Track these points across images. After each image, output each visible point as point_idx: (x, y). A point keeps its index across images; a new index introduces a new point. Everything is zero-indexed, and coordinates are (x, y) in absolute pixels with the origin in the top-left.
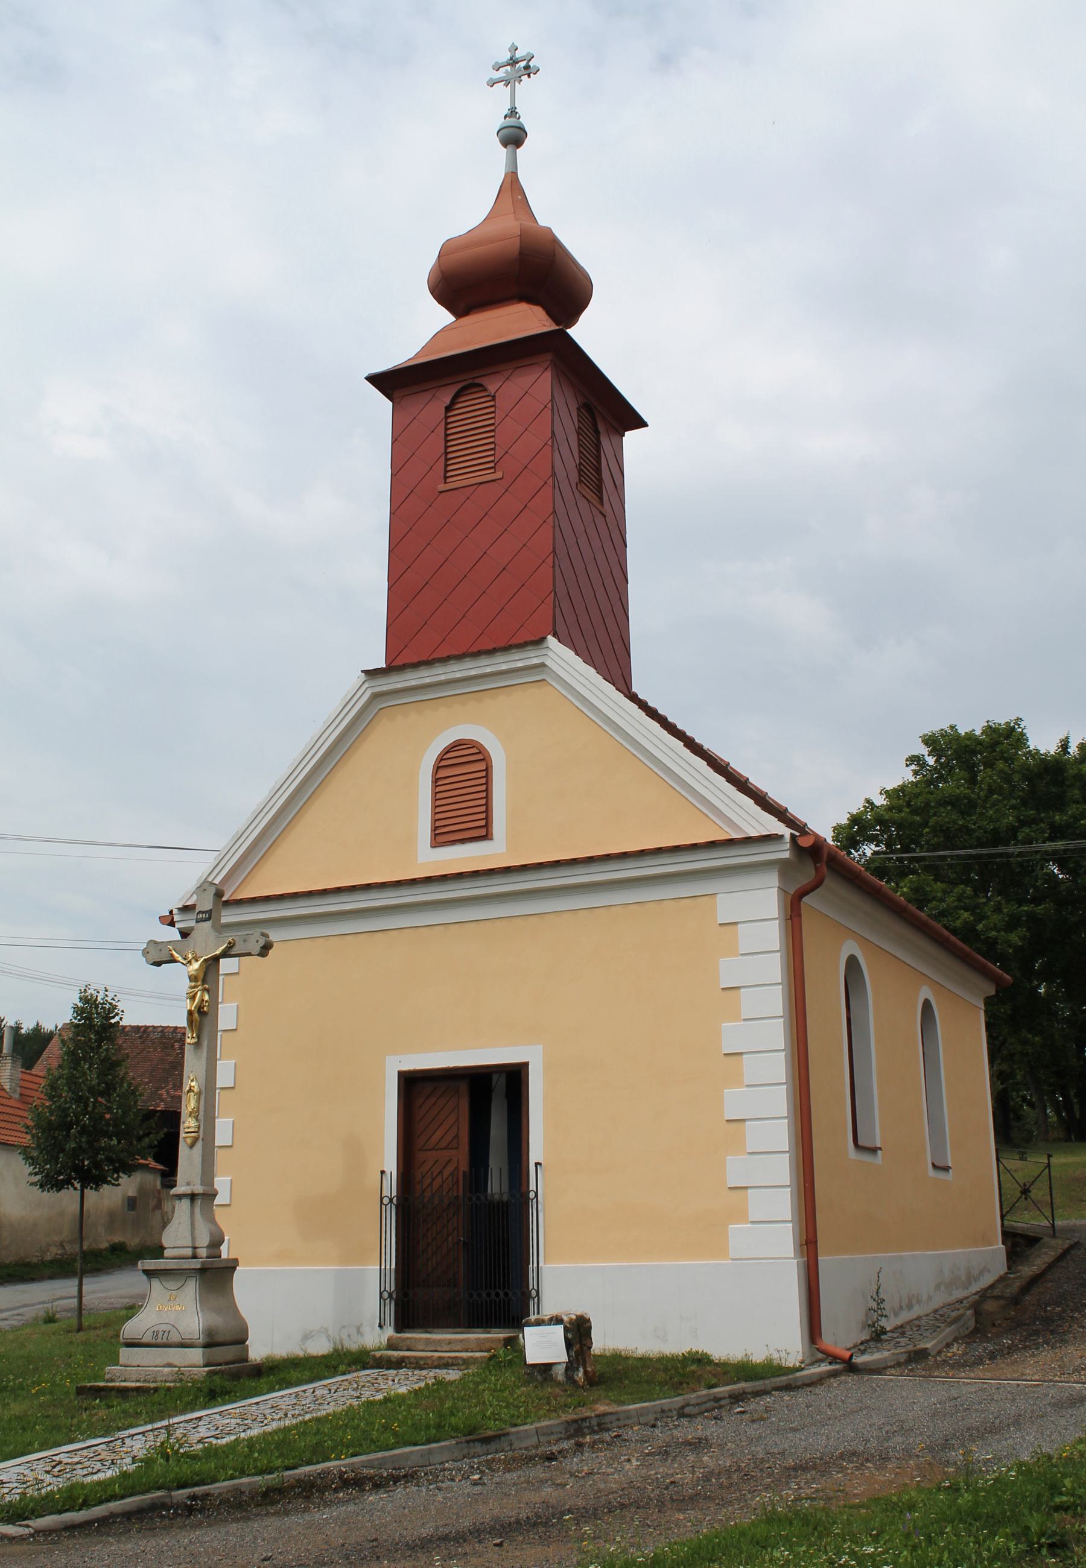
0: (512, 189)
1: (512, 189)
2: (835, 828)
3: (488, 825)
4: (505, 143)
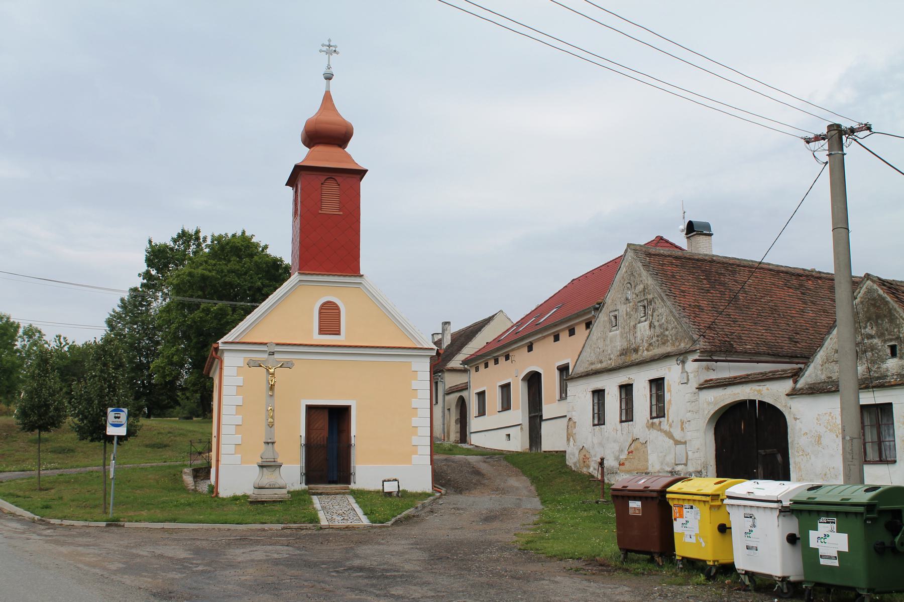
0: (328, 97)
1: (328, 97)
3: (339, 331)
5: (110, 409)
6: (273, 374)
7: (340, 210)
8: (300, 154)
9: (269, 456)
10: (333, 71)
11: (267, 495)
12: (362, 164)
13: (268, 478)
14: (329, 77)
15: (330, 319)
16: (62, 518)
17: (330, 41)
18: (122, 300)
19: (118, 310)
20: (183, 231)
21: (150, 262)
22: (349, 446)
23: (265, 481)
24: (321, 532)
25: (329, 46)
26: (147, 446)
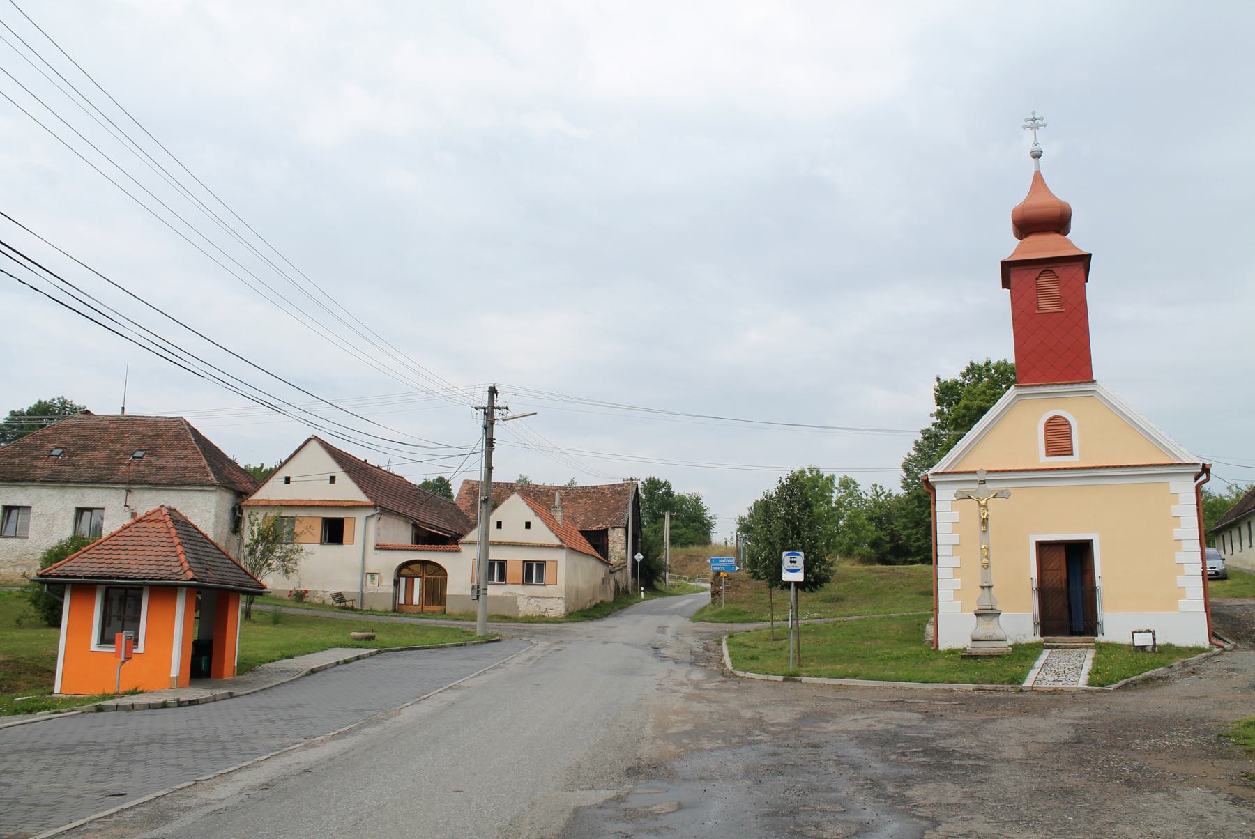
0: (1038, 178)
1: (1038, 178)
2: (13, 413)
4: (1034, 157)
5: (785, 553)
6: (985, 506)
7: (1061, 307)
8: (1009, 246)
9: (986, 603)
10: (1041, 147)
11: (983, 648)
12: (1085, 250)
13: (986, 628)
14: (1037, 155)
15: (1058, 436)
16: (745, 670)
17: (1034, 113)
18: (916, 442)
19: (913, 453)
20: (972, 364)
21: (939, 401)
22: (1093, 590)
23: (981, 633)
24: (1020, 695)
25: (1034, 119)
26: (921, 594)
